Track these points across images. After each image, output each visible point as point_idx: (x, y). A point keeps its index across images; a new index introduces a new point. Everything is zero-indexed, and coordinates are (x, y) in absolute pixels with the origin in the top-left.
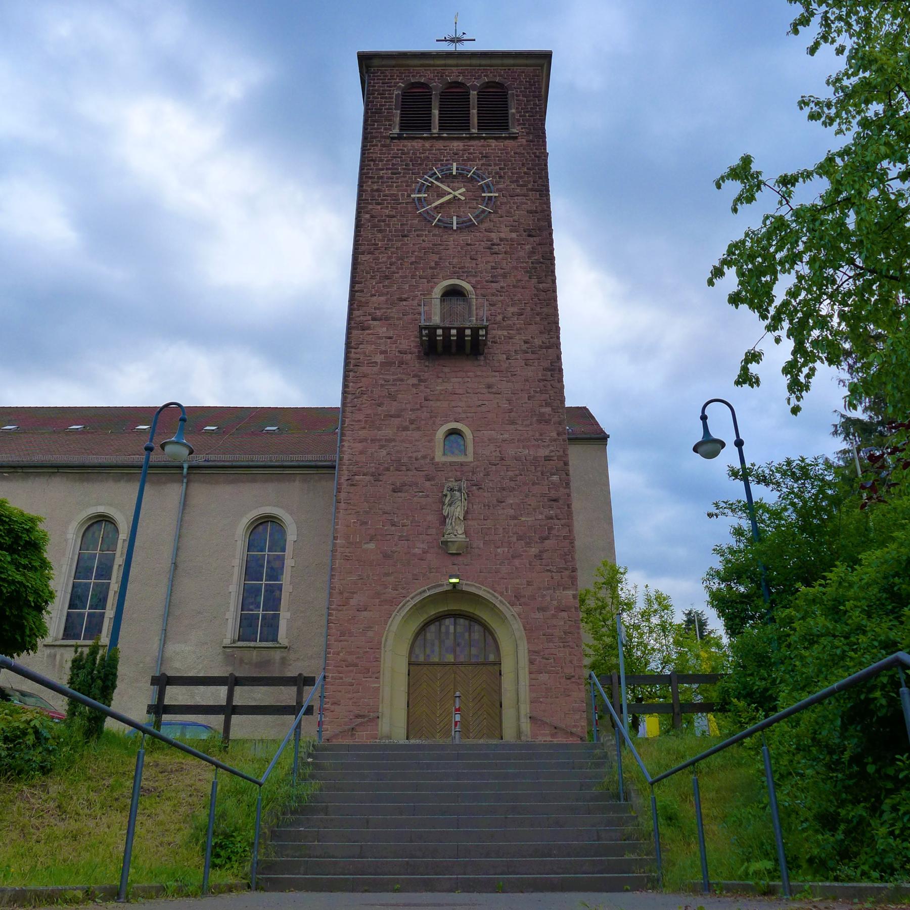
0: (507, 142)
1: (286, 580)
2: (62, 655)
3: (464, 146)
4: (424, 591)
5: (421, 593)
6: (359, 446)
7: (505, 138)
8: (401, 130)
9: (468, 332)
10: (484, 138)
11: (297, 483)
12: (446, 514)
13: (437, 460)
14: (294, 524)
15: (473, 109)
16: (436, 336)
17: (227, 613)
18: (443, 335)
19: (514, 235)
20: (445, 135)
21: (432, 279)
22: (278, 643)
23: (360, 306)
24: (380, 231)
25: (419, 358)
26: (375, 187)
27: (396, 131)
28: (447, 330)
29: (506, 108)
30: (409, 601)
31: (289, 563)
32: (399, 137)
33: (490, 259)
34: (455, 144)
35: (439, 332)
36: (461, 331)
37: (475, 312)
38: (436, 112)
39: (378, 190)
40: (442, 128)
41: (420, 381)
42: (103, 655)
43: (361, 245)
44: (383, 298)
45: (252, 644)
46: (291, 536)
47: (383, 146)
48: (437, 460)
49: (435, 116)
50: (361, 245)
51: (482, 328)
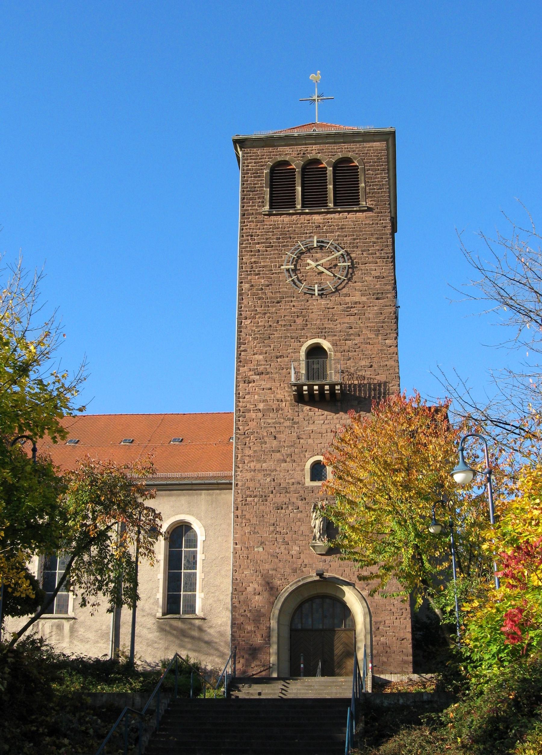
0: (359, 214)
1: (199, 571)
2: (43, 625)
3: (324, 219)
4: (299, 581)
5: (296, 582)
6: (249, 475)
7: (356, 211)
8: (270, 208)
9: (327, 387)
10: (340, 212)
11: (203, 496)
12: (313, 526)
13: (307, 485)
14: (203, 528)
15: (330, 185)
16: (303, 391)
17: (158, 594)
18: (308, 390)
19: (364, 299)
20: (307, 211)
21: (299, 340)
22: (196, 615)
23: (247, 362)
24: (260, 298)
25: (291, 405)
26: (253, 260)
27: (267, 208)
28: (311, 387)
29: (357, 183)
30: (288, 588)
31: (200, 557)
32: (270, 215)
33: (347, 320)
34: (316, 217)
35: (305, 388)
36: (321, 387)
37: (333, 366)
38: (299, 189)
39: (255, 262)
40: (303, 206)
41: (295, 423)
42: (389, 682)
43: (243, 311)
44: (261, 357)
45: (177, 616)
46: (201, 538)
47: (258, 222)
48: (307, 485)
49: (298, 192)
50: (243, 311)
51: (337, 384)
